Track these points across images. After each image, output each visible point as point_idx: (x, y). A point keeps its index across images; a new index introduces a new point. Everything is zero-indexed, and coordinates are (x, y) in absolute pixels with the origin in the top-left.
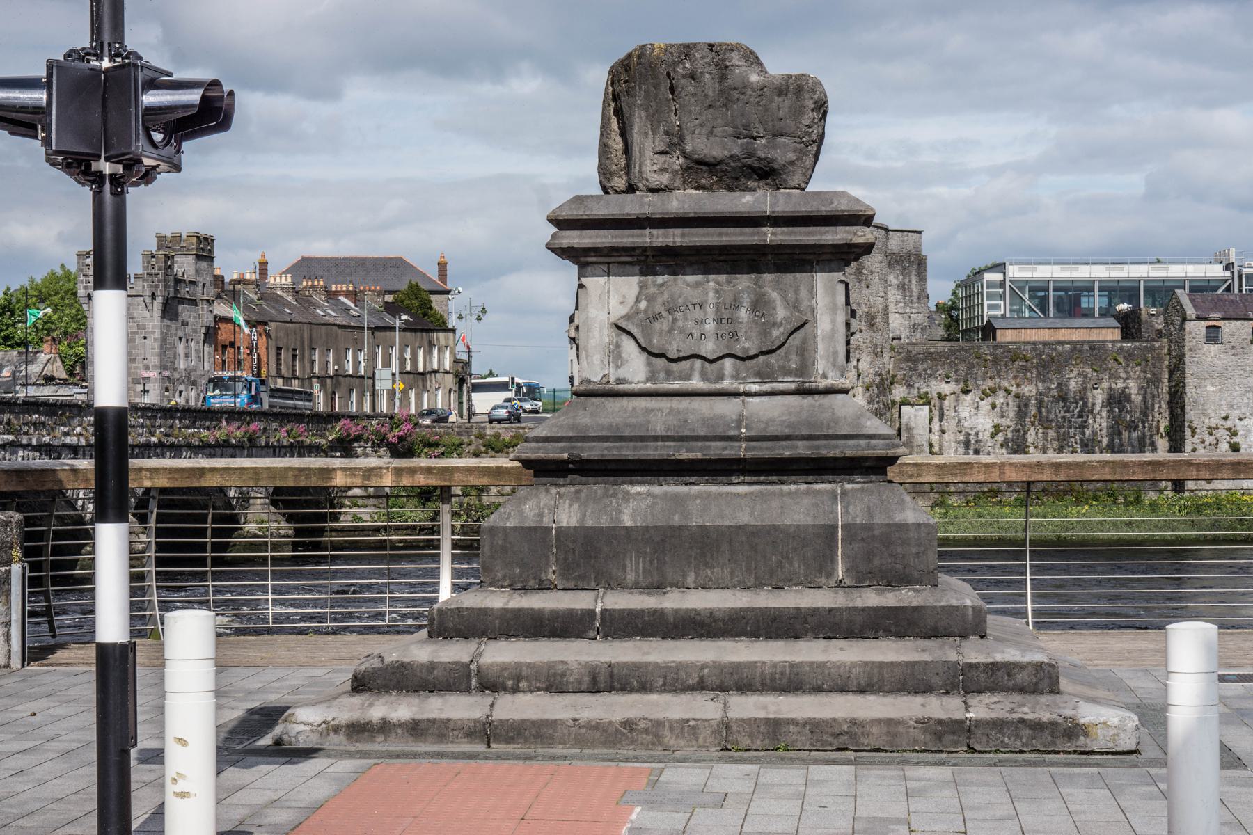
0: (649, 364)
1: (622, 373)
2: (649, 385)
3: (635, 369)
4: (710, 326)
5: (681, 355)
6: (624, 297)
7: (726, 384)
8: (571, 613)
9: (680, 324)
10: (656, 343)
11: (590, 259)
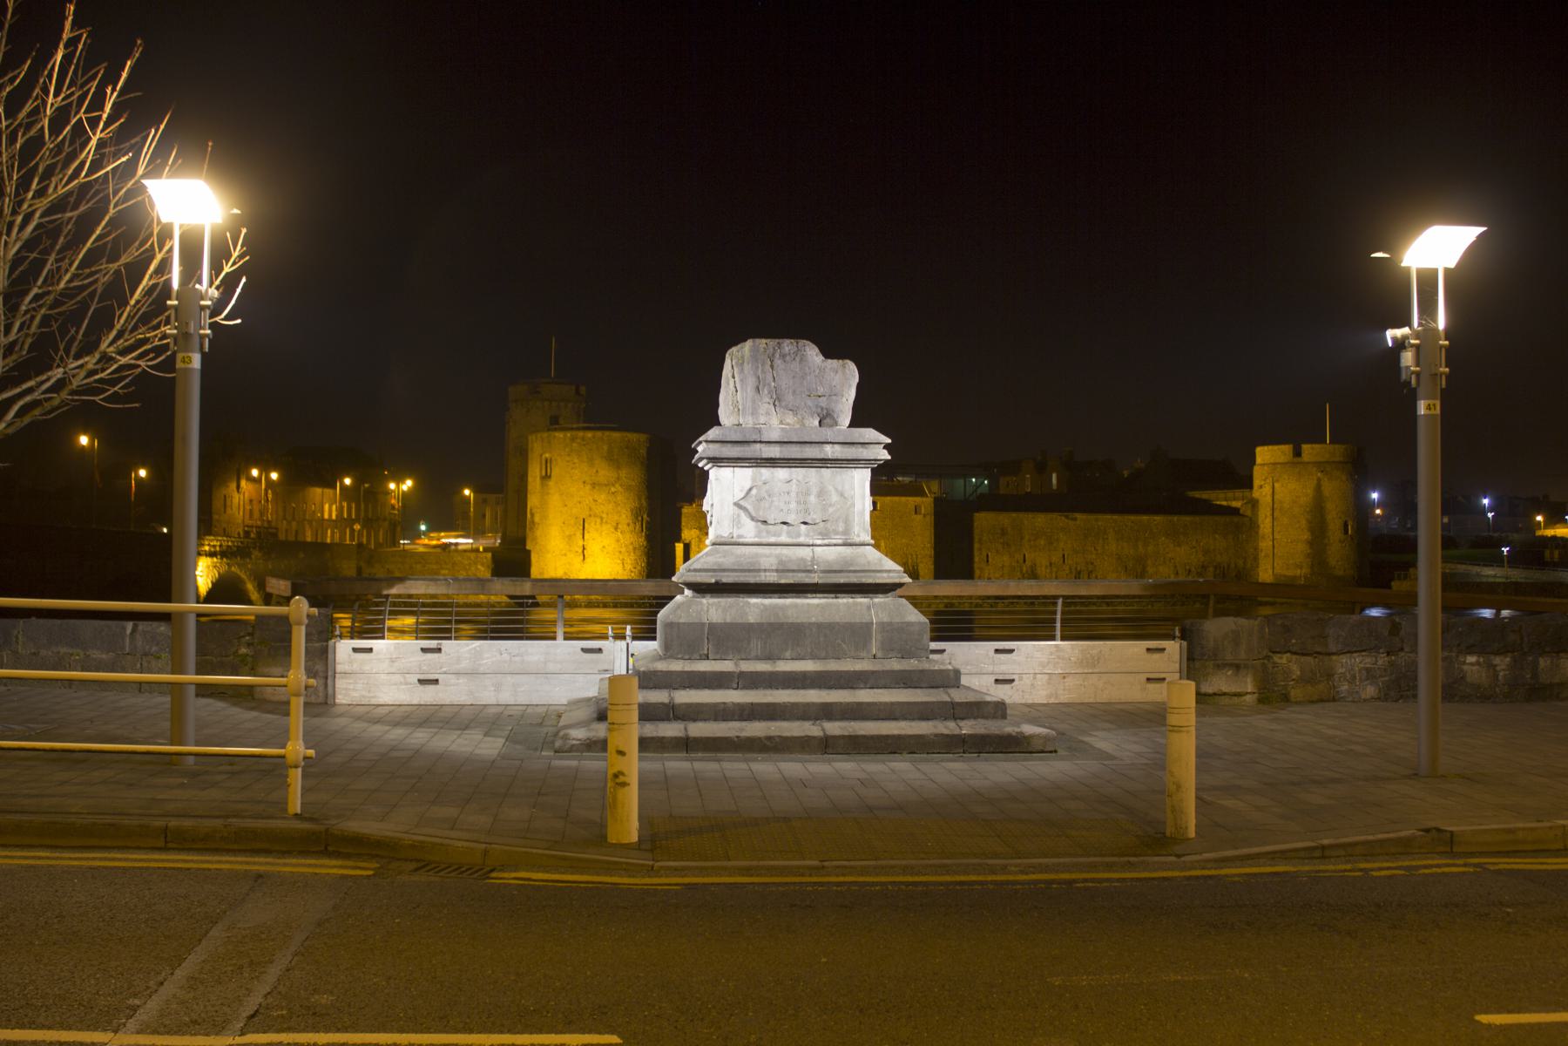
1: (741, 532)
3: (749, 531)
4: (793, 505)
7: (802, 540)
8: (722, 673)
10: (761, 515)
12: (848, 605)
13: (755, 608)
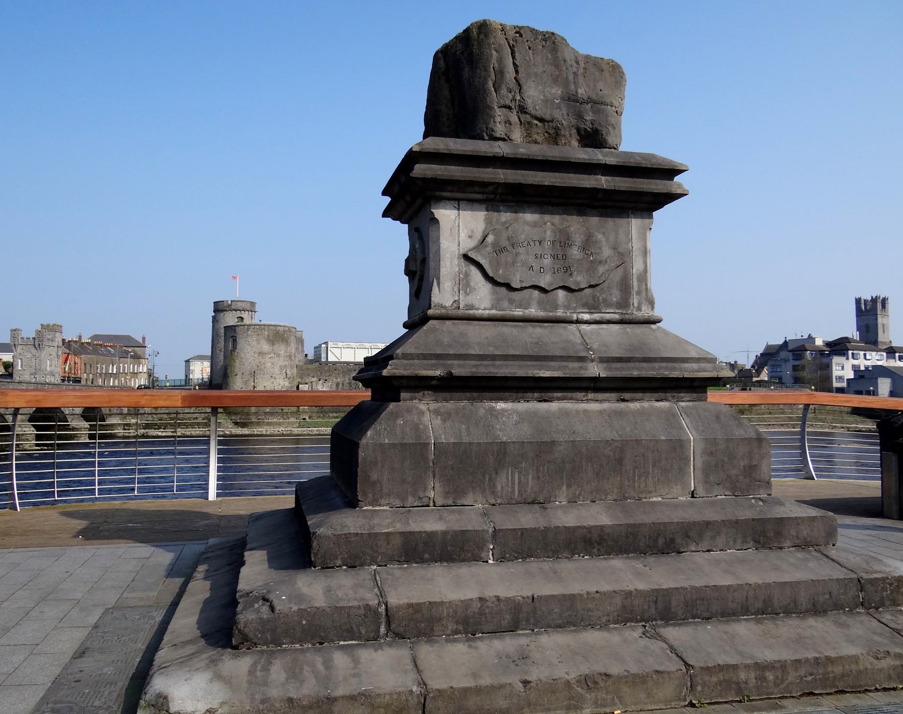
0: (494, 293)
1: (472, 299)
2: (494, 312)
4: (547, 261)
5: (524, 285)
6: (472, 231)
7: (560, 313)
9: (522, 257)
11: (444, 194)
12: (524, 417)
13: (510, 415)
